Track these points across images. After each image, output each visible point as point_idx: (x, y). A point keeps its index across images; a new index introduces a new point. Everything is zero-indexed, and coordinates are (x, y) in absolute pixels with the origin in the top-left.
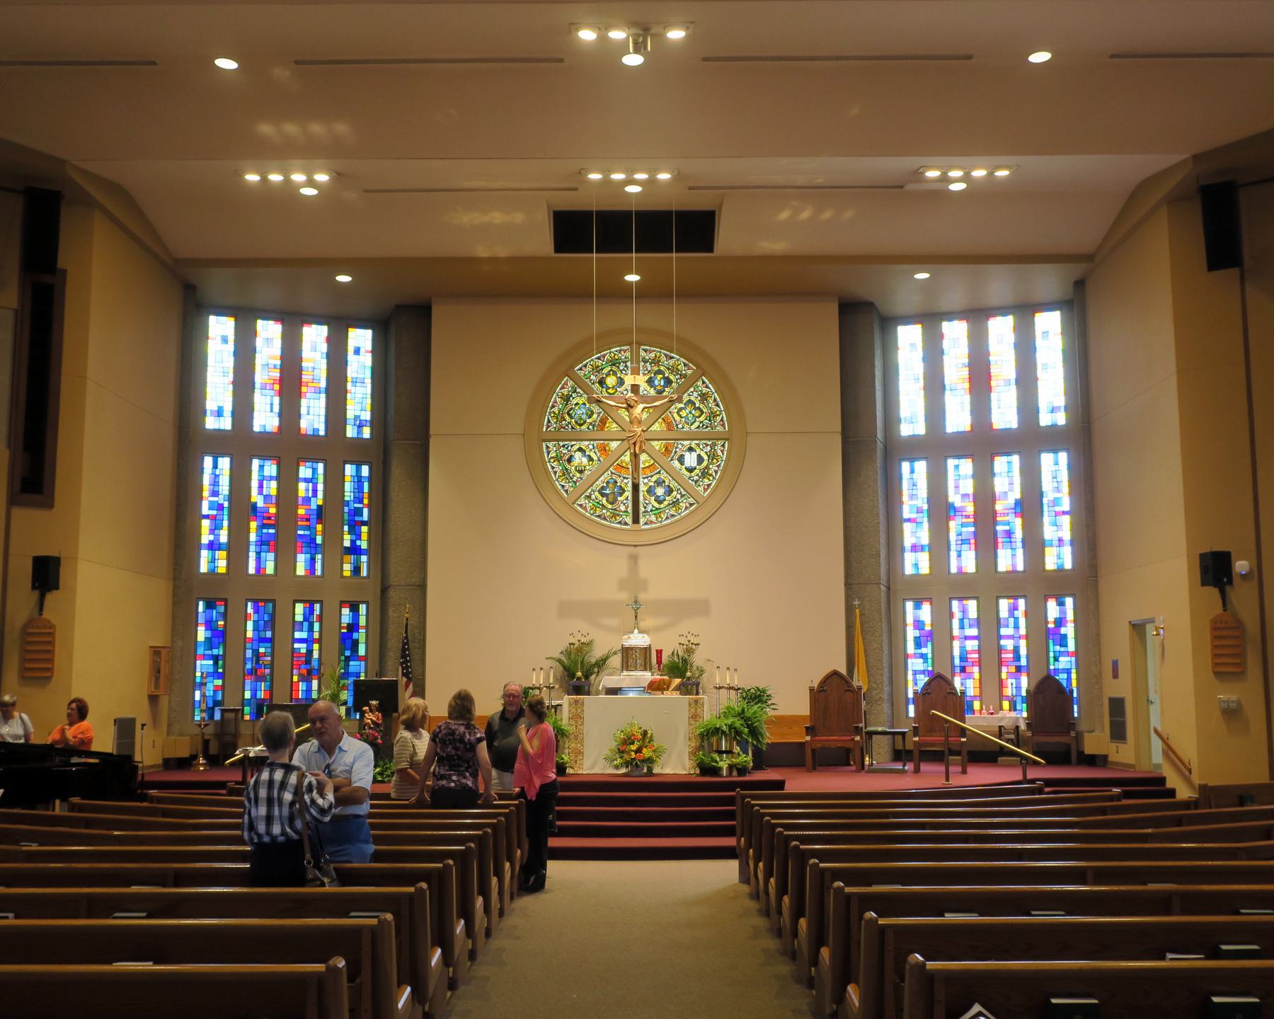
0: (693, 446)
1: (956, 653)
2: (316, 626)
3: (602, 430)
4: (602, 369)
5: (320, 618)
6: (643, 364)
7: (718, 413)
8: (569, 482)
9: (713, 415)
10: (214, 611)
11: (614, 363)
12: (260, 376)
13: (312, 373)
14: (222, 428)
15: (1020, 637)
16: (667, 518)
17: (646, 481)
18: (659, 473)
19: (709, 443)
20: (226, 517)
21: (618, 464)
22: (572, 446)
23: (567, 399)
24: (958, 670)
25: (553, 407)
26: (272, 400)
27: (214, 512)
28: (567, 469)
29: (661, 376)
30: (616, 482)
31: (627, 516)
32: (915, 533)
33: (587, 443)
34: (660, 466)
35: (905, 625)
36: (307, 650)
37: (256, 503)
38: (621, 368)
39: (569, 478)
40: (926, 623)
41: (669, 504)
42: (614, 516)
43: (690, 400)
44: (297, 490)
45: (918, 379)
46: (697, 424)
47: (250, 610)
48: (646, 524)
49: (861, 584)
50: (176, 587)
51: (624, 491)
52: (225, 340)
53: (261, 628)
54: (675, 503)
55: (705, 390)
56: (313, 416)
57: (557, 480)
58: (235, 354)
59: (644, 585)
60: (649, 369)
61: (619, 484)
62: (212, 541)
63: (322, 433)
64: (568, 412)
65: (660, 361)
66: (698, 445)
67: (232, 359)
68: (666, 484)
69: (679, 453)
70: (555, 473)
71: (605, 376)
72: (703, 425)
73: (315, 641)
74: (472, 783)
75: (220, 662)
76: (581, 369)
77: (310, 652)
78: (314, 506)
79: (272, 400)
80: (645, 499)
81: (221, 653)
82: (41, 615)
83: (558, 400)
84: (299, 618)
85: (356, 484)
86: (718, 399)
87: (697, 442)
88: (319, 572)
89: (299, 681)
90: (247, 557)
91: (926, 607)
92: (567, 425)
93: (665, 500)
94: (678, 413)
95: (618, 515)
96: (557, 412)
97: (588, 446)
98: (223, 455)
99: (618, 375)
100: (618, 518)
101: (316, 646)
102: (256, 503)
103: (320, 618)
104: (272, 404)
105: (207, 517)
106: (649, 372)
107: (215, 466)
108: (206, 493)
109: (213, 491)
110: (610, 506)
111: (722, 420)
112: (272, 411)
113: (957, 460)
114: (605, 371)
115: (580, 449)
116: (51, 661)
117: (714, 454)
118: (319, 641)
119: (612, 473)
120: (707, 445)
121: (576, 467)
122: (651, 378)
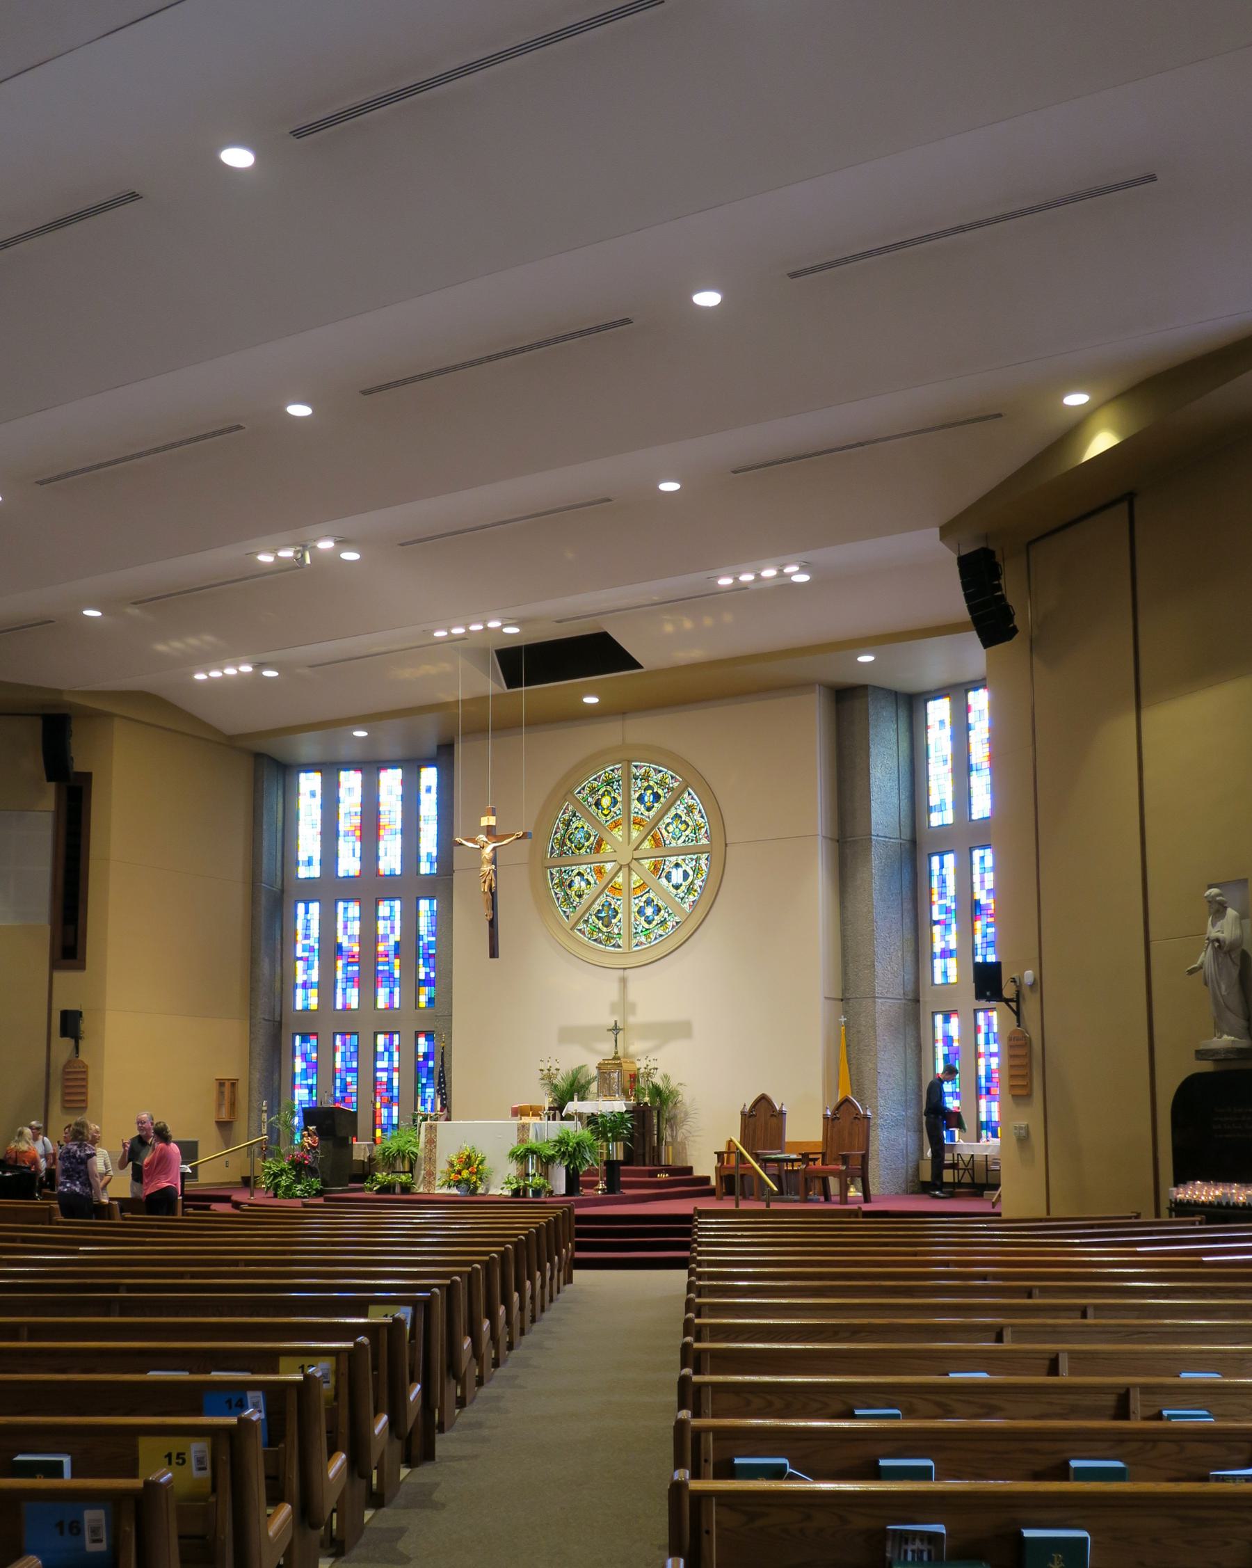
0: (679, 862)
1: (982, 1072)
2: (396, 1055)
3: (598, 852)
4: (598, 790)
5: (398, 1048)
6: (634, 780)
7: (702, 825)
8: (570, 907)
9: (698, 828)
11: (609, 783)
15: (985, 1055)
16: (656, 939)
17: (637, 901)
19: (695, 857)
20: (316, 958)
21: (612, 886)
22: (572, 871)
23: (568, 824)
24: (984, 1092)
25: (556, 833)
26: (354, 846)
28: (568, 895)
29: (651, 791)
30: (610, 904)
31: (620, 938)
32: (306, 972)
35: (934, 1041)
37: (342, 943)
38: (615, 787)
40: (954, 1038)
41: (658, 924)
42: (609, 938)
43: (677, 814)
45: (947, 760)
46: (683, 839)
47: (338, 1043)
48: (637, 945)
49: (857, 998)
52: (313, 794)
53: (348, 1059)
54: (663, 922)
55: (691, 802)
56: (390, 860)
57: (560, 906)
60: (640, 785)
61: (613, 907)
62: (306, 981)
63: (398, 872)
64: (569, 837)
66: (684, 860)
68: (655, 903)
69: (667, 870)
70: (558, 899)
71: (600, 797)
73: (394, 1070)
74: (80, 1190)
75: (314, 1091)
76: (579, 792)
77: (390, 1080)
78: (392, 943)
79: (354, 846)
80: (636, 920)
81: (315, 1083)
82: (78, 1057)
84: (380, 1048)
85: (429, 918)
87: (683, 857)
88: (397, 1005)
89: (381, 1108)
90: (335, 993)
91: (954, 1021)
92: (568, 851)
93: (653, 920)
95: (613, 938)
96: (559, 838)
97: (586, 869)
98: (313, 901)
99: (612, 795)
100: (612, 941)
101: (396, 1075)
102: (342, 943)
103: (398, 1048)
104: (354, 850)
105: (301, 959)
106: (640, 788)
107: (307, 912)
108: (299, 937)
110: (605, 929)
112: (354, 856)
113: (982, 851)
114: (601, 792)
115: (579, 874)
116: (85, 1094)
118: (398, 1070)
119: (607, 896)
120: (692, 859)
121: (576, 892)
122: (641, 794)
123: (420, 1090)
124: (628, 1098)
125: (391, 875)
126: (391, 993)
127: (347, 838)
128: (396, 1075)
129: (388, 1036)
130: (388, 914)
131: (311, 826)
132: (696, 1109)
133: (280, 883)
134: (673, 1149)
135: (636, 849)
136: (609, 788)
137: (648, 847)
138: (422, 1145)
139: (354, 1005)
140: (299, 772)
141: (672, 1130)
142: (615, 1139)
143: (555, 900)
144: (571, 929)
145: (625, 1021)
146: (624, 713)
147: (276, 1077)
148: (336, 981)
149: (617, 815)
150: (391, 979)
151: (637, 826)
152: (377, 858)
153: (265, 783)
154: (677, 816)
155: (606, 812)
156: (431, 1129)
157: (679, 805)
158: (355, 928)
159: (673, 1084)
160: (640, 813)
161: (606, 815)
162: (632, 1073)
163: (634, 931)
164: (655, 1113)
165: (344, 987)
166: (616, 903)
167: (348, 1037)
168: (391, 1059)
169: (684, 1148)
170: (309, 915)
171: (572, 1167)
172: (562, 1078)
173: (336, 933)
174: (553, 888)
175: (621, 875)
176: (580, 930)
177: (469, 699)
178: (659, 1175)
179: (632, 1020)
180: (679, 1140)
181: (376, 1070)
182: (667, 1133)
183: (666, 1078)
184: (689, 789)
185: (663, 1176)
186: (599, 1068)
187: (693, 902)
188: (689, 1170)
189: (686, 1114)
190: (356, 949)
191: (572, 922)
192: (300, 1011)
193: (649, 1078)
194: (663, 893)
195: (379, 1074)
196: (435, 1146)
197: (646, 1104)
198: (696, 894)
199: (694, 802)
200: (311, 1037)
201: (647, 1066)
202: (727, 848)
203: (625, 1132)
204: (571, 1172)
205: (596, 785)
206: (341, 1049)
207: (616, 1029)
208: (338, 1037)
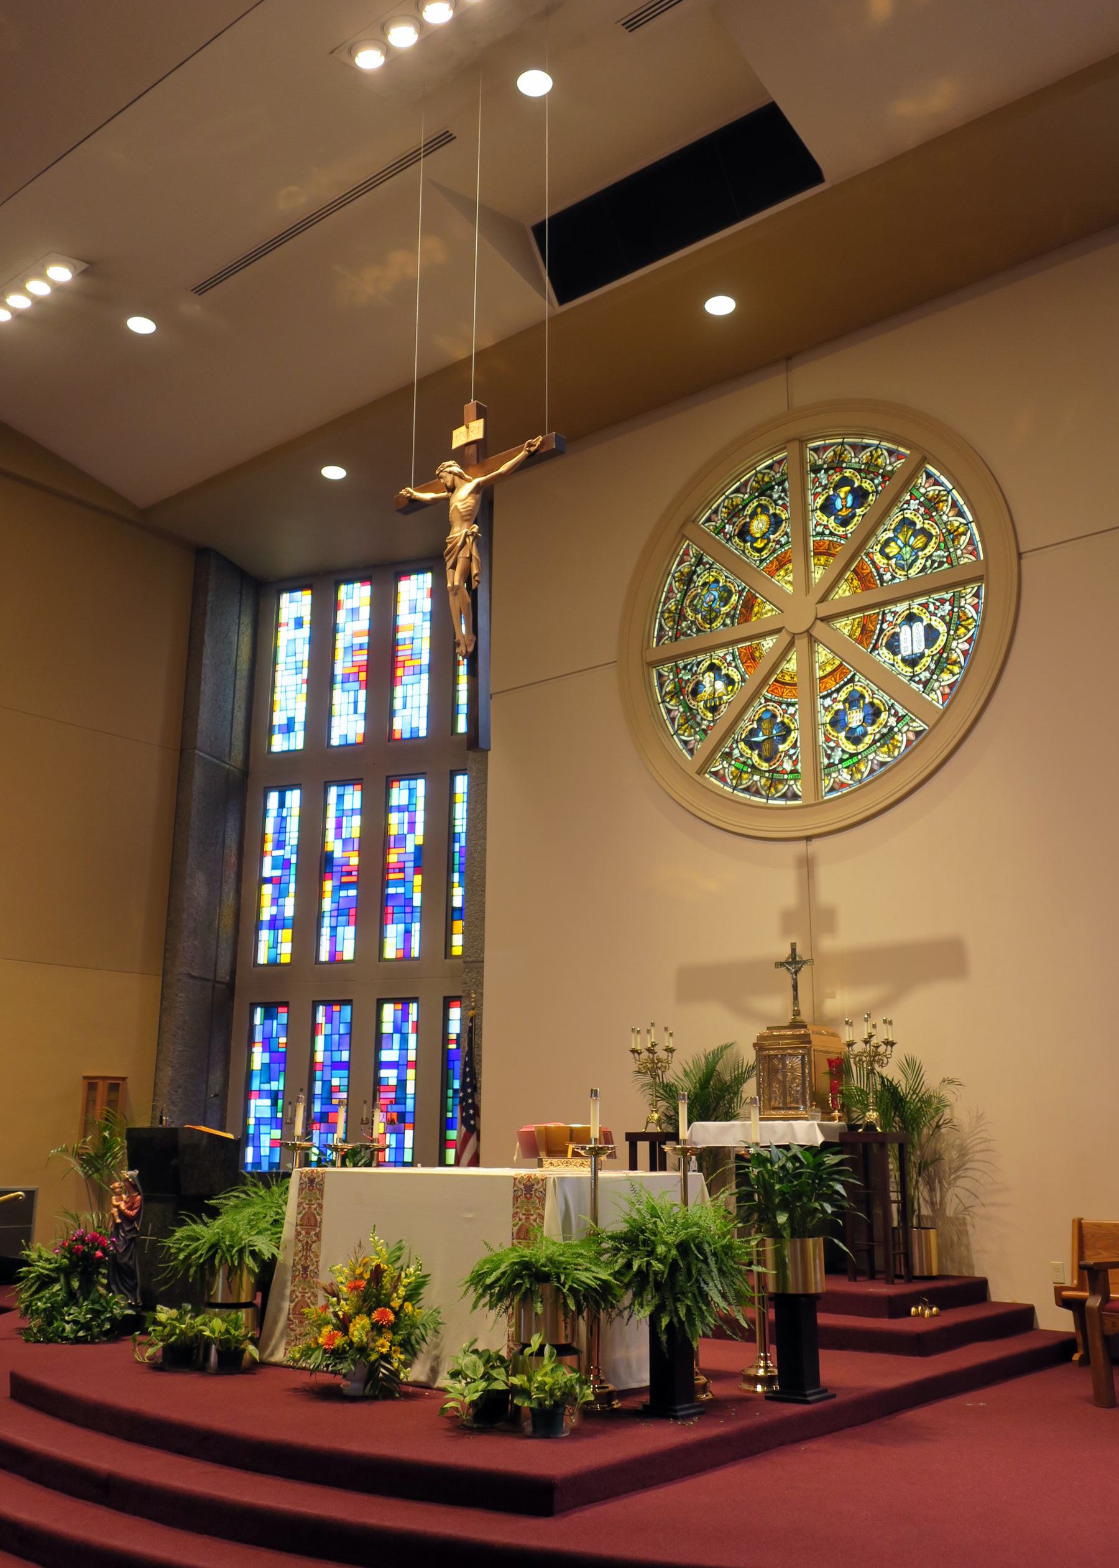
0: (915, 611)
2: (412, 1039)
4: (744, 507)
5: (417, 1025)
6: (813, 476)
7: (961, 529)
8: (696, 733)
10: (275, 1022)
12: (342, 666)
13: (410, 646)
14: (292, 748)
17: (828, 702)
18: (852, 680)
19: (948, 596)
20: (293, 878)
21: (776, 681)
22: (699, 664)
23: (688, 580)
25: (667, 598)
27: (278, 873)
28: (691, 709)
29: (847, 489)
30: (774, 716)
31: (795, 780)
33: (721, 653)
34: (853, 668)
36: (398, 1081)
37: (332, 852)
38: (775, 496)
39: (695, 725)
41: (874, 742)
42: (773, 783)
44: (387, 825)
46: (919, 565)
47: (321, 1018)
48: (832, 789)
50: (164, 985)
51: (789, 731)
54: (887, 736)
55: (932, 491)
58: (311, 640)
59: (827, 920)
60: (824, 482)
61: (779, 720)
62: (276, 915)
63: (423, 733)
65: (843, 461)
66: (925, 606)
67: (307, 647)
68: (867, 700)
70: (673, 720)
71: (748, 520)
72: (933, 562)
73: (409, 1065)
75: (280, 1102)
76: (709, 520)
77: (402, 1082)
78: (410, 848)
80: (828, 740)
81: (281, 1088)
83: (676, 585)
84: (387, 1027)
86: (961, 501)
87: (922, 600)
88: (415, 953)
90: (318, 936)
92: (690, 628)
93: (865, 734)
94: (882, 552)
95: (781, 781)
98: (291, 787)
99: (771, 512)
100: (780, 787)
102: (332, 852)
104: (356, 703)
107: (282, 804)
108: (269, 846)
109: (279, 841)
110: (765, 766)
111: (971, 542)
112: (356, 712)
114: (748, 511)
115: (712, 667)
117: (959, 617)
118: (414, 1065)
119: (767, 700)
121: (706, 702)
122: (828, 498)
123: (450, 1101)
124: (827, 1114)
125: (411, 738)
126: (408, 933)
127: (347, 685)
128: (411, 1074)
129: (400, 1007)
130: (404, 801)
131: (294, 671)
132: (987, 1141)
133: (240, 757)
134: (938, 1235)
135: (823, 599)
136: (764, 500)
137: (847, 594)
138: (288, 1231)
139: (348, 954)
140: (279, 593)
141: (932, 1190)
142: (799, 1230)
143: (667, 722)
144: (699, 773)
145: (812, 946)
146: (789, 358)
147: (216, 1077)
148: (320, 915)
149: (782, 546)
150: (408, 909)
151: (823, 559)
152: (392, 713)
153: (210, 594)
154: (907, 523)
155: (759, 544)
156: (312, 1185)
157: (908, 502)
158: (353, 826)
159: (931, 1082)
160: (827, 532)
161: (760, 551)
162: (834, 1056)
163: (826, 761)
164: (893, 1151)
165: (334, 924)
166: (785, 712)
167: (336, 1008)
168: (404, 1047)
169: (963, 1233)
170: (285, 810)
171: (665, 1321)
172: (685, 1071)
173: (324, 836)
174: (663, 701)
175: (794, 657)
176: (715, 774)
177: (492, 347)
178: (913, 1310)
179: (828, 944)
180: (949, 1212)
181: (380, 1065)
182: (921, 1194)
183: (911, 1066)
184: (930, 468)
185: (925, 1316)
186: (759, 1047)
187: (951, 686)
188: (977, 1290)
189: (963, 1152)
190: (354, 861)
191: (700, 757)
192: (264, 965)
193: (876, 1066)
194: (884, 679)
195: (384, 1073)
196: (318, 1235)
197: (870, 1127)
198: (956, 669)
199: (941, 488)
200: (280, 1010)
201: (871, 1036)
202: (1023, 561)
203: (829, 1209)
204: (664, 1338)
205: (739, 501)
206: (326, 1029)
207: (794, 963)
208: (321, 1010)
